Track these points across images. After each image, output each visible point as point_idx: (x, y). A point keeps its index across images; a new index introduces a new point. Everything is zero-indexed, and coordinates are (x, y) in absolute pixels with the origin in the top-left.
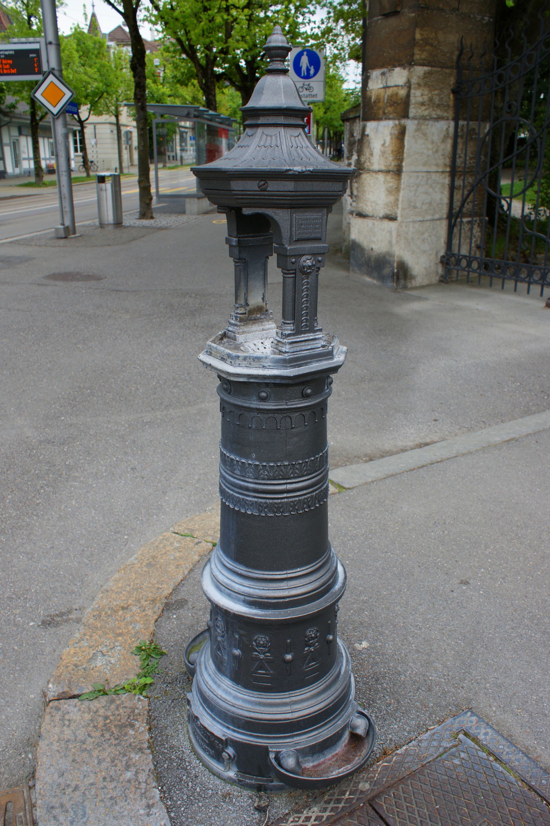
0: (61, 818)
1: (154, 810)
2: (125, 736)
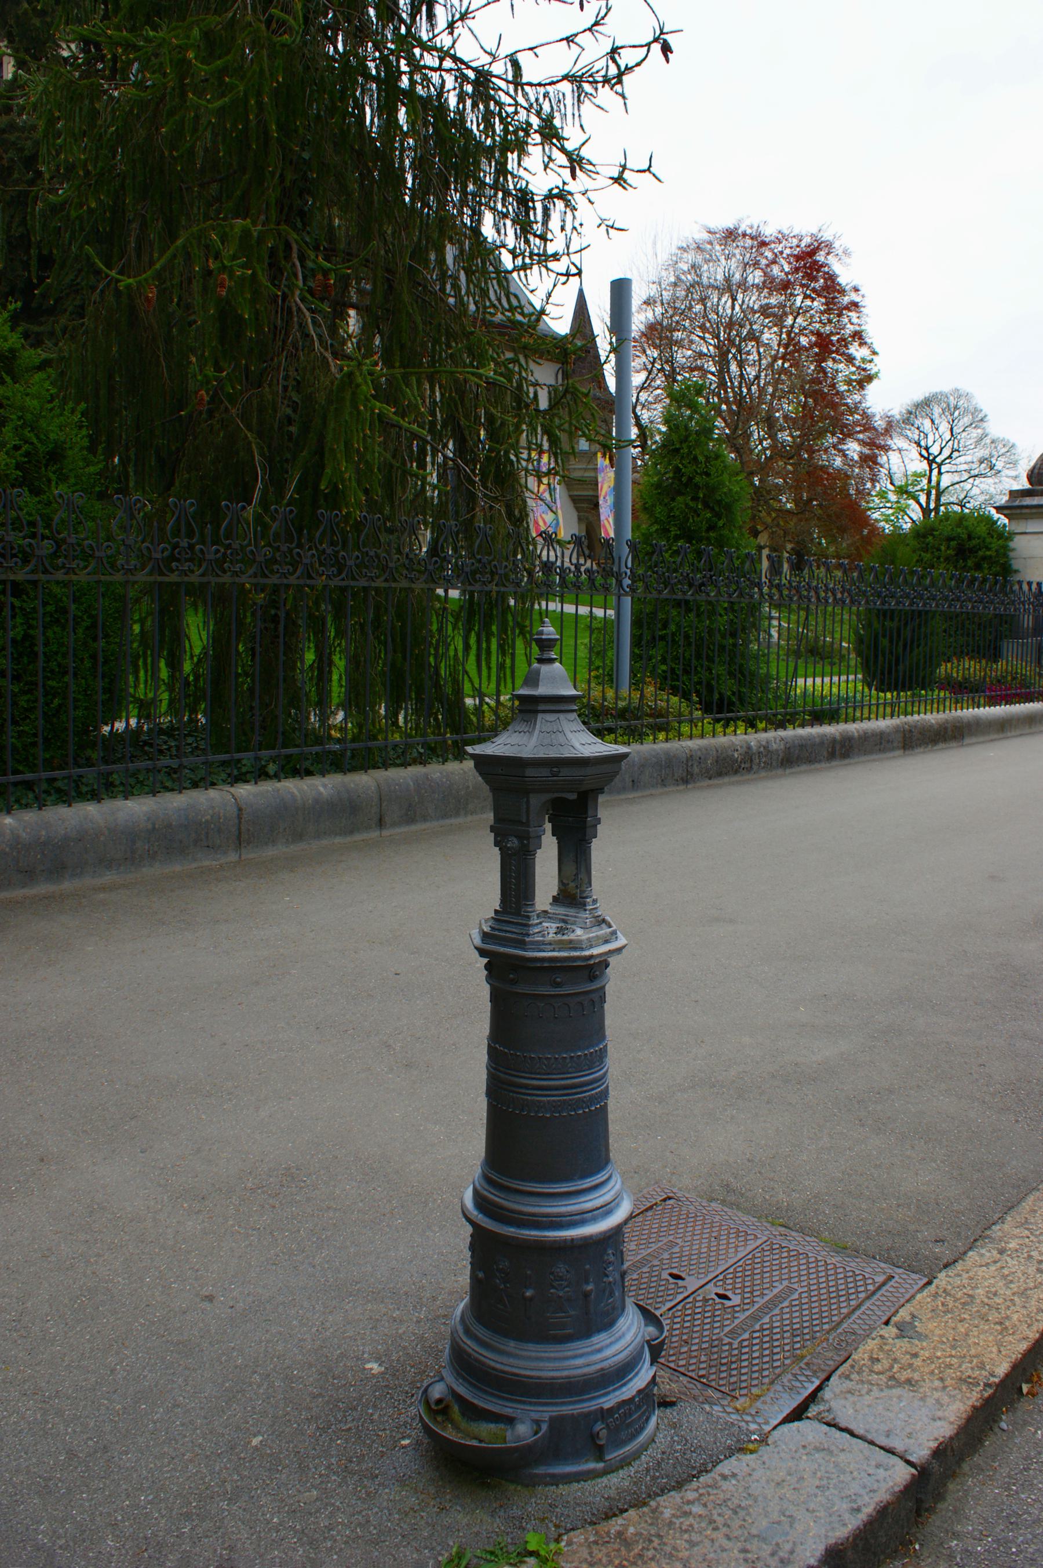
0: (788, 1547)
1: (727, 1472)
2: (642, 1534)
